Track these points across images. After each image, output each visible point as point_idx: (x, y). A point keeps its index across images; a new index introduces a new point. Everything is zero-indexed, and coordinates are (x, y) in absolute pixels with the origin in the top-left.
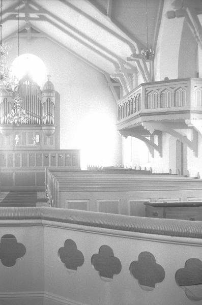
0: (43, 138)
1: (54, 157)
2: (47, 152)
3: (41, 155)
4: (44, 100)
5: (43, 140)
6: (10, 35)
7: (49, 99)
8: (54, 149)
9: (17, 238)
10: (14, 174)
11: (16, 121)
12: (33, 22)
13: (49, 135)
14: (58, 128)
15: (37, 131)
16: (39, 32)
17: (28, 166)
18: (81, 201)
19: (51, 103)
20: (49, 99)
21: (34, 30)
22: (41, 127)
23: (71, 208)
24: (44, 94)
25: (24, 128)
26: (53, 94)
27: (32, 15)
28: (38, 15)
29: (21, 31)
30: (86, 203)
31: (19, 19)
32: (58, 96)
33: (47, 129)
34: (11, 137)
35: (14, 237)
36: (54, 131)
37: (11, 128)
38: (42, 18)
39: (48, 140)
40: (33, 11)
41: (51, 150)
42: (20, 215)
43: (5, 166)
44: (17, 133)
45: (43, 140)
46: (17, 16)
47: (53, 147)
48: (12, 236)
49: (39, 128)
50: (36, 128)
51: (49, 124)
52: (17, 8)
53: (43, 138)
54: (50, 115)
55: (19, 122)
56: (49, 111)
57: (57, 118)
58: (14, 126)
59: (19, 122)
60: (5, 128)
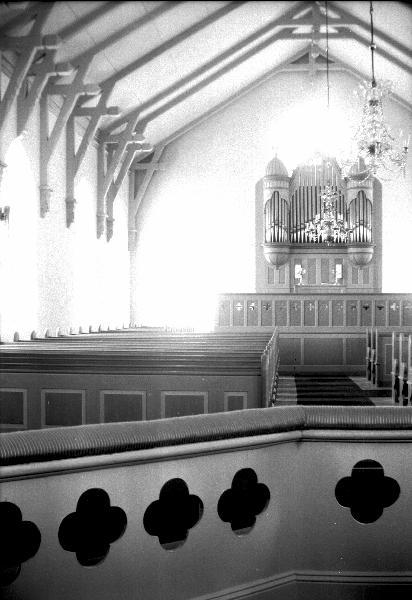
0: (350, 270)
1: (380, 308)
2: (367, 298)
3: (285, 302)
4: (352, 195)
5: (350, 276)
6: (276, 69)
7: (362, 193)
8: (372, 291)
9: (384, 468)
10: (302, 341)
11: (324, 237)
12: (322, 42)
13: (361, 263)
14: (378, 249)
15: (337, 256)
16: (293, 63)
17: (245, 325)
18: (13, 390)
19: (366, 200)
20: (362, 193)
21: (326, 59)
22: (346, 248)
23: (213, 412)
24: (350, 185)
25: (315, 251)
26: (371, 184)
27: (323, 29)
28: (336, 28)
29: (302, 59)
30: (203, 396)
31: (300, 36)
32: (377, 186)
33: (357, 253)
34: (287, 268)
35: (380, 466)
36: (371, 256)
37: (287, 250)
38: (344, 33)
39: (360, 273)
40: (327, 21)
41: (318, 294)
42: (349, 420)
43: (397, 324)
44: (299, 262)
45: (350, 276)
46: (295, 32)
47: (369, 287)
48: (375, 464)
49: (341, 251)
50: (337, 251)
51: (362, 243)
52: (296, 17)
53: (350, 270)
54: (364, 224)
55: (330, 239)
56: (361, 218)
57: (377, 231)
58: (291, 248)
59: (330, 239)
60: (276, 250)
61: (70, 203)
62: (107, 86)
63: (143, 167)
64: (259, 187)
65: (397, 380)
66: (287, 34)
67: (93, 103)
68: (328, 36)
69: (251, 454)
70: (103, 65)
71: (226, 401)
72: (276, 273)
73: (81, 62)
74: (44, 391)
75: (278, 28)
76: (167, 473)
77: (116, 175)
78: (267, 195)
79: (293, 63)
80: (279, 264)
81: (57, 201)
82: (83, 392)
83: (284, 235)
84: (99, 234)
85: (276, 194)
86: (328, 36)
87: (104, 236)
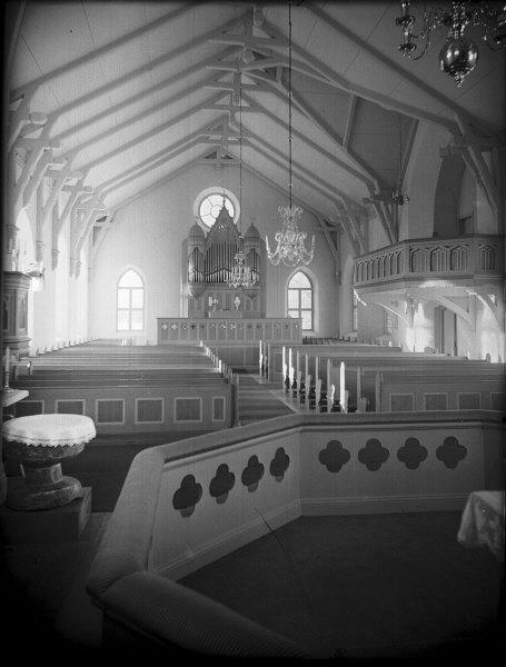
16: (207, 157)
29: (212, 155)
34: (202, 299)
38: (241, 142)
61: (55, 253)
62: (85, 170)
63: (99, 224)
64: (185, 243)
65: (288, 379)
66: (206, 140)
67: (73, 182)
68: (230, 142)
69: (280, 440)
70: (81, 159)
71: (57, 406)
72: (196, 302)
73: (68, 156)
74: (214, 398)
75: (337, 197)
76: (410, 434)
77: (82, 233)
78: (190, 250)
79: (207, 157)
80: (197, 295)
81: (47, 252)
82: (97, 401)
83: (201, 277)
84: (71, 273)
85: (196, 250)
86: (230, 142)
87: (74, 275)
